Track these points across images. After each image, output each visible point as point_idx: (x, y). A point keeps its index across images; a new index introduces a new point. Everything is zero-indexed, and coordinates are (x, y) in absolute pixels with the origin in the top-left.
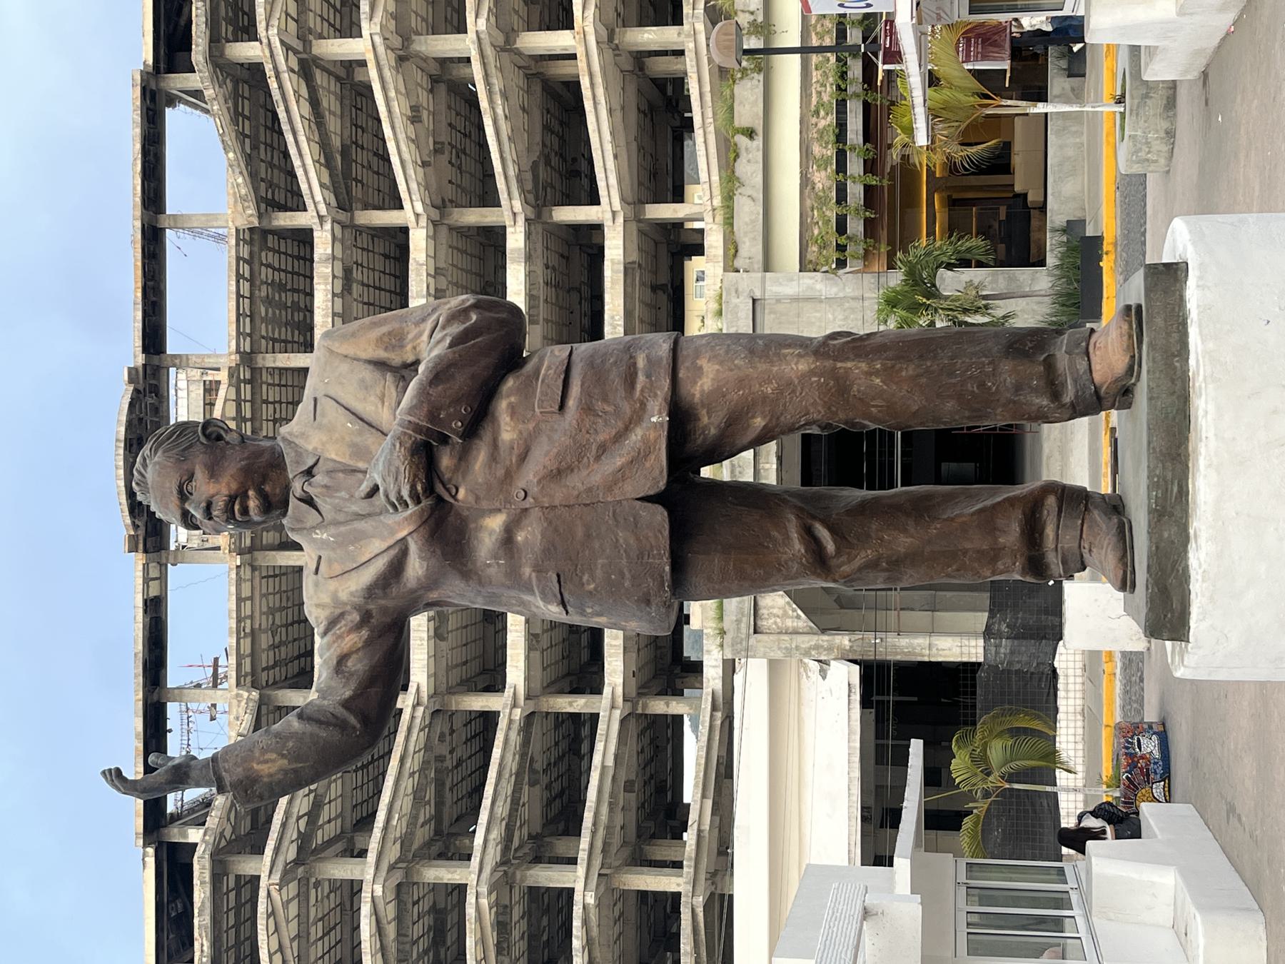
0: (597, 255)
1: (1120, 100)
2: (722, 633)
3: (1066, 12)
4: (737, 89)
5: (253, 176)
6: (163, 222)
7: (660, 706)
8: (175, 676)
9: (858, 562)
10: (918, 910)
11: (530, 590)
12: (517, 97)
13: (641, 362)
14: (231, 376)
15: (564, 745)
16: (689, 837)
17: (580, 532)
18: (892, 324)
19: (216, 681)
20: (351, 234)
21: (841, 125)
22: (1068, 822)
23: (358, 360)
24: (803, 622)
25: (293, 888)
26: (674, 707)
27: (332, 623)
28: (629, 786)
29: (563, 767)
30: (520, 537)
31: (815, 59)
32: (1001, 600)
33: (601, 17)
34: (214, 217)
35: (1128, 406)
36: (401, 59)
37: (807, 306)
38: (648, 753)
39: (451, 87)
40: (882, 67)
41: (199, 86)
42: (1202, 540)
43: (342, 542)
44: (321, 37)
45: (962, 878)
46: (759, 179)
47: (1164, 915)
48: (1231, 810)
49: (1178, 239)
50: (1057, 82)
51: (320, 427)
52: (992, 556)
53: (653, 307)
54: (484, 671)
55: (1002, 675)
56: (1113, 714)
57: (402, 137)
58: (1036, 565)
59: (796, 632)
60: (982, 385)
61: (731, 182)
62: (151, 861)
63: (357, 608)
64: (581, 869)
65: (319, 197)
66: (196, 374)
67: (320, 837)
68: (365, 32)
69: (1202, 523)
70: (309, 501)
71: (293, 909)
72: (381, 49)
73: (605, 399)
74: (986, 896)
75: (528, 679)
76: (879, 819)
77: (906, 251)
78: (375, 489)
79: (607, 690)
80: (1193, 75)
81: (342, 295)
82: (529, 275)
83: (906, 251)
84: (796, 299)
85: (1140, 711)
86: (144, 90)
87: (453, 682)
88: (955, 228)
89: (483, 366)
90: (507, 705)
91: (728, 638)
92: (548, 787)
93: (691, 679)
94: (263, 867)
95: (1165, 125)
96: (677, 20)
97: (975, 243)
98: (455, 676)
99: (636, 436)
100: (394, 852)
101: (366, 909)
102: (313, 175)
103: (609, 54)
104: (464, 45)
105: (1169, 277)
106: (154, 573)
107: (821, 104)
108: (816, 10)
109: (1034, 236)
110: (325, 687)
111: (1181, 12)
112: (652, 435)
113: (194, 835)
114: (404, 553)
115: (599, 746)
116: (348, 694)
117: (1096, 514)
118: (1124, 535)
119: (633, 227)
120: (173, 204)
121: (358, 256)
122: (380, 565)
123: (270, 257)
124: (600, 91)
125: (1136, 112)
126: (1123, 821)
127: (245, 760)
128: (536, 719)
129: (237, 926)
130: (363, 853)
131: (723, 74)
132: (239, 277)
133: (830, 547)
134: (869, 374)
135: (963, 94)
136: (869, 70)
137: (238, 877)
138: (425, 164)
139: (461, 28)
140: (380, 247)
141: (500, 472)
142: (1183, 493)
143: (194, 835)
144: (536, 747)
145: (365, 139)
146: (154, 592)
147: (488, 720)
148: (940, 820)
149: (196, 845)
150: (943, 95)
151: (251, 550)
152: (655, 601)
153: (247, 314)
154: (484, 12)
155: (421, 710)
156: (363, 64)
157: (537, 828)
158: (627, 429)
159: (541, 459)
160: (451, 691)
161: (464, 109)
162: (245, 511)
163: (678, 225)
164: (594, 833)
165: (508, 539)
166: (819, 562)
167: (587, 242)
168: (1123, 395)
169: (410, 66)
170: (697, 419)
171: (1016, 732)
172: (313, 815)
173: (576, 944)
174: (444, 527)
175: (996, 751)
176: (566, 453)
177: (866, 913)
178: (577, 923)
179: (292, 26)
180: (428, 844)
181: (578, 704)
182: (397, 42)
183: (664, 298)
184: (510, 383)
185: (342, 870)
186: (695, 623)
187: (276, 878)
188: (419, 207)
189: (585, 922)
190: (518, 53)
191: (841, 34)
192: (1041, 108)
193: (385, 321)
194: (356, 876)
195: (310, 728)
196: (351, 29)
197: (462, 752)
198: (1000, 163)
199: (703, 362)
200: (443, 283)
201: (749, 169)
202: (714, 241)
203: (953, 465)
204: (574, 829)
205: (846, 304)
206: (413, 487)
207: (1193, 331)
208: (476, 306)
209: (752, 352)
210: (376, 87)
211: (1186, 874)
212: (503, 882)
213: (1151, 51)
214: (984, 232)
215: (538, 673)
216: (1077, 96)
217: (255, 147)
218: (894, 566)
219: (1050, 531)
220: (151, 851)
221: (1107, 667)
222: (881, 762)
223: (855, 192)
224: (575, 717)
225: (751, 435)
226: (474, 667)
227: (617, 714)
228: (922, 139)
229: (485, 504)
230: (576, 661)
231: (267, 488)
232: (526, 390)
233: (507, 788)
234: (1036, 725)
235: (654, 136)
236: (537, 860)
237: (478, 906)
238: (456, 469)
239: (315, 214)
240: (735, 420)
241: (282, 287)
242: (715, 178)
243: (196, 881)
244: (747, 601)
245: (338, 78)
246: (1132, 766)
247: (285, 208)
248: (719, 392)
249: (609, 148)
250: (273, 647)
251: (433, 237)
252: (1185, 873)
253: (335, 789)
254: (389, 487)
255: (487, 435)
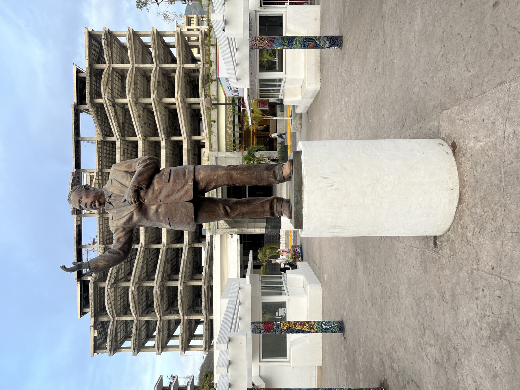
0: (181, 147)
1: (291, 117)
2: (210, 229)
3: (280, 98)
4: (211, 112)
5: (101, 129)
6: (80, 139)
7: (197, 245)
8: (84, 243)
9: (235, 214)
10: (251, 287)
11: (162, 222)
12: (163, 113)
13: (187, 171)
14: (97, 174)
15: (175, 255)
16: (203, 273)
17: (173, 209)
18: (245, 163)
19: (94, 243)
20: (125, 142)
21: (234, 120)
22: (282, 266)
23: (121, 171)
24: (227, 226)
25: (113, 289)
26: (200, 245)
27: (116, 231)
28: (190, 263)
29: (175, 260)
30: (160, 210)
31: (228, 106)
32: (268, 221)
33: (181, 96)
34: (92, 138)
35: (291, 180)
36: (136, 104)
37: (228, 159)
38: (194, 256)
39: (147, 110)
40: (242, 108)
41: (88, 108)
42: (305, 208)
43: (118, 212)
44: (117, 98)
45: (261, 279)
46: (216, 132)
47: (302, 285)
48: (315, 263)
49: (300, 146)
50: (278, 113)
51: (113, 186)
52: (264, 212)
53: (194, 159)
54: (157, 239)
55: (269, 236)
56: (291, 243)
57: (136, 121)
58: (272, 214)
59: (226, 229)
60: (260, 176)
61: (210, 132)
62: (79, 285)
63: (122, 227)
64: (179, 282)
65: (117, 134)
66: (88, 174)
67: (119, 277)
68: (128, 97)
69: (305, 205)
70: (110, 203)
71: (113, 294)
72: (131, 101)
73: (179, 180)
74: (266, 283)
75: (167, 241)
76: (243, 267)
77: (248, 148)
78: (125, 200)
79: (185, 242)
80: (305, 112)
81: (123, 156)
82: (166, 152)
83: (248, 148)
84: (225, 157)
85: (296, 243)
86: (74, 109)
87: (150, 242)
88: (258, 143)
89: (150, 172)
90: (162, 246)
91: (211, 230)
92: (172, 264)
93: (204, 239)
94: (106, 285)
95: (300, 122)
96: (198, 97)
97: (262, 146)
98: (150, 240)
99: (186, 187)
100: (137, 280)
101: (130, 293)
102: (116, 129)
103: (183, 104)
104: (150, 101)
105: (298, 154)
106: (79, 219)
107: (229, 116)
108: (227, 96)
109: (274, 144)
110: (115, 246)
111: (303, 98)
112: (190, 187)
113: (89, 278)
114: (133, 214)
115: (183, 255)
116: (120, 246)
117: (284, 203)
118: (290, 207)
119: (189, 141)
120: (82, 135)
121: (126, 147)
122: (127, 217)
123: (106, 147)
124: (181, 112)
125: (294, 119)
126: (293, 266)
127: (95, 262)
128: (169, 250)
129: (100, 298)
130: (129, 281)
131: (208, 109)
132: (98, 152)
133: (229, 211)
134: (237, 174)
135: (259, 115)
136: (239, 109)
137: (100, 287)
138: (142, 127)
139: (150, 97)
140: (131, 145)
141: (155, 196)
142: (301, 198)
143: (89, 278)
144: (169, 255)
145: (128, 121)
146: (79, 223)
147: (158, 250)
148: (256, 267)
149: (89, 281)
150: (255, 115)
151: (102, 213)
152: (191, 224)
153: (101, 160)
154: (155, 94)
155: (142, 248)
156: (127, 104)
157: (169, 273)
158: (184, 186)
159: (164, 193)
160: (149, 244)
161: (150, 115)
162: (95, 206)
163: (199, 141)
164: (182, 274)
165: (157, 211)
166: (227, 214)
167: (179, 144)
168: (289, 178)
169: (138, 105)
170: (199, 184)
171: (271, 248)
172: (118, 273)
173: (179, 298)
174: (142, 208)
175: (268, 252)
176: (171, 192)
177: (240, 288)
178: (179, 293)
179: (110, 95)
180: (145, 278)
181: (178, 246)
182: (135, 100)
183: (196, 158)
184: (157, 176)
185: (125, 284)
186: (204, 227)
187: (109, 287)
188: (140, 137)
189: (180, 293)
190: (163, 103)
191: (234, 101)
192: (275, 118)
193: (128, 162)
194: (128, 286)
195: (111, 254)
196: (124, 97)
197: (152, 257)
198: (267, 129)
199: (201, 171)
200: (146, 153)
201: (214, 129)
202: (207, 144)
203: (259, 193)
204: (177, 273)
205: (236, 158)
206: (134, 200)
207: (303, 165)
208: (148, 159)
209: (211, 169)
210: (130, 110)
211: (306, 276)
212: (162, 285)
213: (297, 106)
214: (264, 144)
215: (169, 239)
216: (283, 116)
217: (102, 122)
218: (243, 215)
219: (275, 207)
220: (79, 282)
221: (290, 234)
222: (244, 255)
223: (237, 134)
224: (178, 248)
225: (212, 187)
226: (155, 238)
227: (187, 248)
228: (250, 124)
229: (151, 203)
230: (178, 237)
231: (100, 200)
232: (161, 177)
233: (163, 265)
234: (275, 247)
235: (194, 122)
236: (170, 280)
237: (156, 291)
238: (144, 195)
239: (116, 137)
240: (208, 184)
241: (108, 154)
242: (207, 131)
243: (90, 289)
244: (215, 223)
245: (121, 107)
246: (295, 254)
247: (109, 136)
248: (204, 178)
249: (183, 124)
250: (108, 235)
251: (144, 143)
252: (306, 276)
253: (123, 267)
254: (129, 200)
255: (151, 188)
